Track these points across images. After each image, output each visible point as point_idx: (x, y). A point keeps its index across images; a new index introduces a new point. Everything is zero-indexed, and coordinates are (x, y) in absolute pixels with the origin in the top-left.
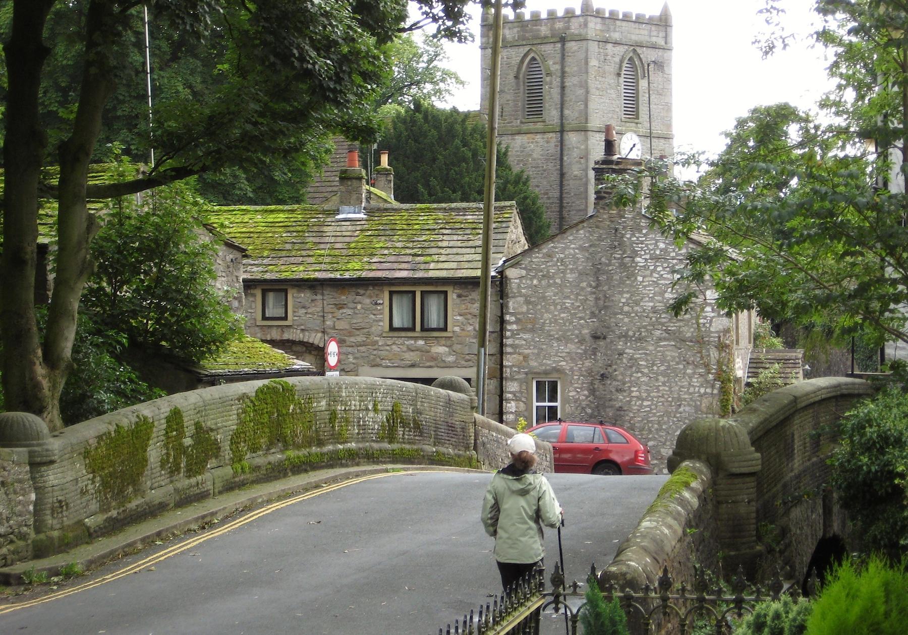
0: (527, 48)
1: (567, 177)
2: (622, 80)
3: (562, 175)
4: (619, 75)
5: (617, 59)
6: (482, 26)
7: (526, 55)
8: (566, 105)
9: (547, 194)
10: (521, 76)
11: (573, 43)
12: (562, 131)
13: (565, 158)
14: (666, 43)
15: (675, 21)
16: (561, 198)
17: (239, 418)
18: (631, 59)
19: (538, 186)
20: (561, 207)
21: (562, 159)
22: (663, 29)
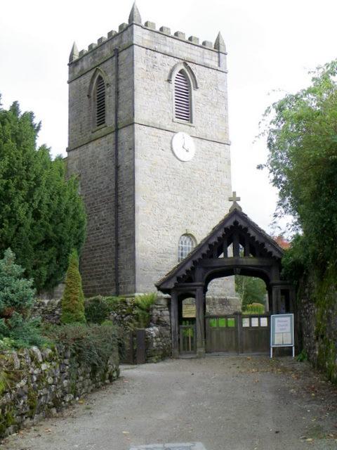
0: (91, 73)
1: (121, 168)
2: (173, 86)
3: (117, 168)
4: (169, 81)
5: (168, 69)
6: (69, 65)
7: (94, 76)
8: (120, 106)
9: (108, 187)
10: (92, 94)
11: (124, 52)
12: (117, 130)
13: (120, 153)
14: (219, 66)
15: (228, 45)
16: (117, 188)
17: (19, 264)
18: (181, 72)
19: (102, 183)
20: (117, 196)
21: (117, 154)
22: (217, 54)
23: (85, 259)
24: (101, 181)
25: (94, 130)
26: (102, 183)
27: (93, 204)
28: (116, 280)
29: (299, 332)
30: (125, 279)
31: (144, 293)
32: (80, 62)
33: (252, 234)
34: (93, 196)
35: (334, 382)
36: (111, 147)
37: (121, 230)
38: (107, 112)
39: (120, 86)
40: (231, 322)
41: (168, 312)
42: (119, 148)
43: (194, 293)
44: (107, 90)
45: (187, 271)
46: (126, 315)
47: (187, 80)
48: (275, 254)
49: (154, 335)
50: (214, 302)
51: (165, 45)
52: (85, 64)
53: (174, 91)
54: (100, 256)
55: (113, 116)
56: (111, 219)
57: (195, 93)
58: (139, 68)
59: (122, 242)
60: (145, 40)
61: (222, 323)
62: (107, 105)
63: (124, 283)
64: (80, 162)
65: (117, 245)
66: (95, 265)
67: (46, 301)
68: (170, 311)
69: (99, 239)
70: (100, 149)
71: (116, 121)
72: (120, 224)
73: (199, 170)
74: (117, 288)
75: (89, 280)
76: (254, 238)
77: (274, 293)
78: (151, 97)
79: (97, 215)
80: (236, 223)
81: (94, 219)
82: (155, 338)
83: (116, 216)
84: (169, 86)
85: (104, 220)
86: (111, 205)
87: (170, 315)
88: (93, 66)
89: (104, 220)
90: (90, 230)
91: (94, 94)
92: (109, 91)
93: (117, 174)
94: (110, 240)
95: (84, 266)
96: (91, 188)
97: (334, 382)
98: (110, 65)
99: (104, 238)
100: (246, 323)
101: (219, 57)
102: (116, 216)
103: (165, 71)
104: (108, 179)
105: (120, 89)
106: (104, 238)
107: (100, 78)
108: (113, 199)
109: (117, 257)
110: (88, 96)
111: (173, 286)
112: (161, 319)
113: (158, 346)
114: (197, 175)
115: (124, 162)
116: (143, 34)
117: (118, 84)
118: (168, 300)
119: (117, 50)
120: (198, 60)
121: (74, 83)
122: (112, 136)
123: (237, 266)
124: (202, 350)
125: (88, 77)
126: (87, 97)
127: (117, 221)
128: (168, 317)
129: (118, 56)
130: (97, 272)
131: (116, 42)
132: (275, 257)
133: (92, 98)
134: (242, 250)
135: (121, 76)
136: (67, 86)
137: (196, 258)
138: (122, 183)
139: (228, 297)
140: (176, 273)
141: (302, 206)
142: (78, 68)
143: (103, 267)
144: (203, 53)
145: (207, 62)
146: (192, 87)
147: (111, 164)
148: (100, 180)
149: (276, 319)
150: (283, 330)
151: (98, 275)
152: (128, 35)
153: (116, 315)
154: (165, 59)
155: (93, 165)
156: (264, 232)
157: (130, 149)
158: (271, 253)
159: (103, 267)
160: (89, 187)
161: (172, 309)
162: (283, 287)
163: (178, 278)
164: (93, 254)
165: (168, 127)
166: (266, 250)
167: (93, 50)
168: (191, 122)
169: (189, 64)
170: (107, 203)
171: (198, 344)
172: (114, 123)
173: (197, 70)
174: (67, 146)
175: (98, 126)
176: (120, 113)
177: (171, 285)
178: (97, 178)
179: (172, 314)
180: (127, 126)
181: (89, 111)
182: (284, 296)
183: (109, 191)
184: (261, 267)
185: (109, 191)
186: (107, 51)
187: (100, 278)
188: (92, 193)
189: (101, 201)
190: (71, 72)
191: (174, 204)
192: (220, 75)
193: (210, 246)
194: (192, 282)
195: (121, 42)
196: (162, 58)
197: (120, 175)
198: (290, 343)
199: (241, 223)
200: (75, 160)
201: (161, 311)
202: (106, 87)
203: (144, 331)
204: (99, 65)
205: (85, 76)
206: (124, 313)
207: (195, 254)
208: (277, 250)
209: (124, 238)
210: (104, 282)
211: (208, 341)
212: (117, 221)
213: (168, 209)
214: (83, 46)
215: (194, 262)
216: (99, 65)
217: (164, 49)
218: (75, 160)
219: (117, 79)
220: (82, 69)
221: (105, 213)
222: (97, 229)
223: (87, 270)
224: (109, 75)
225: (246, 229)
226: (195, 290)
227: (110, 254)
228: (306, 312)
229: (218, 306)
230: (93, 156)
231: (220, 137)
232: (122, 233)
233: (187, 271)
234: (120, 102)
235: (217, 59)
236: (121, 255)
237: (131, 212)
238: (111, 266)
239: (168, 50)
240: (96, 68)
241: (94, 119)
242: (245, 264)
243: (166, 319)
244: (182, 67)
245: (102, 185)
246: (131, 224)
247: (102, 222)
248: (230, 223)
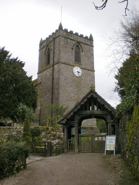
1: (54, 79)
2: (74, 51)
3: (53, 79)
7: (47, 48)
12: (53, 65)
16: (53, 86)
19: (48, 84)
20: (53, 89)
21: (53, 74)
26: (48, 84)
29: (118, 143)
33: (99, 100)
38: (50, 60)
41: (63, 134)
43: (74, 125)
44: (51, 52)
45: (71, 116)
46: (49, 134)
48: (109, 109)
49: (55, 144)
50: (85, 128)
51: (71, 36)
52: (44, 44)
53: (74, 52)
55: (52, 61)
56: (50, 97)
57: (82, 54)
61: (86, 138)
62: (50, 57)
68: (64, 133)
70: (48, 73)
71: (53, 62)
72: (51, 100)
76: (100, 102)
77: (108, 126)
80: (92, 96)
82: (56, 145)
85: (48, 97)
87: (64, 135)
89: (48, 97)
92: (52, 52)
93: (53, 81)
99: (48, 104)
100: (96, 139)
104: (50, 83)
105: (55, 51)
107: (49, 48)
108: (51, 90)
111: (65, 122)
112: (60, 136)
114: (82, 82)
117: (54, 50)
120: (84, 42)
121: (41, 51)
123: (93, 114)
124: (77, 150)
125: (45, 49)
127: (52, 98)
128: (63, 136)
129: (54, 40)
131: (54, 36)
132: (109, 110)
134: (96, 109)
135: (55, 47)
136: (38, 52)
137: (75, 111)
140: (67, 117)
141: (111, 158)
144: (85, 40)
145: (86, 43)
147: (51, 77)
148: (47, 83)
149: (108, 138)
150: (110, 142)
153: (44, 133)
156: (104, 100)
158: (107, 109)
161: (65, 132)
162: (113, 124)
163: (67, 119)
166: (105, 107)
167: (47, 39)
171: (76, 148)
172: (52, 63)
173: (82, 45)
176: (55, 59)
177: (64, 122)
179: (65, 135)
181: (45, 60)
182: (113, 127)
184: (103, 115)
186: (51, 39)
193: (81, 106)
195: (56, 35)
197: (54, 81)
199: (94, 96)
201: (60, 133)
203: (51, 142)
206: (47, 133)
207: (75, 109)
208: (110, 107)
211: (80, 147)
212: (52, 98)
215: (74, 112)
217: (70, 37)
219: (54, 48)
220: (43, 46)
225: (96, 98)
226: (75, 124)
228: (122, 135)
229: (89, 130)
231: (90, 69)
233: (71, 116)
239: (72, 38)
241: (46, 62)
242: (96, 113)
243: (62, 136)
244: (77, 44)
248: (90, 96)
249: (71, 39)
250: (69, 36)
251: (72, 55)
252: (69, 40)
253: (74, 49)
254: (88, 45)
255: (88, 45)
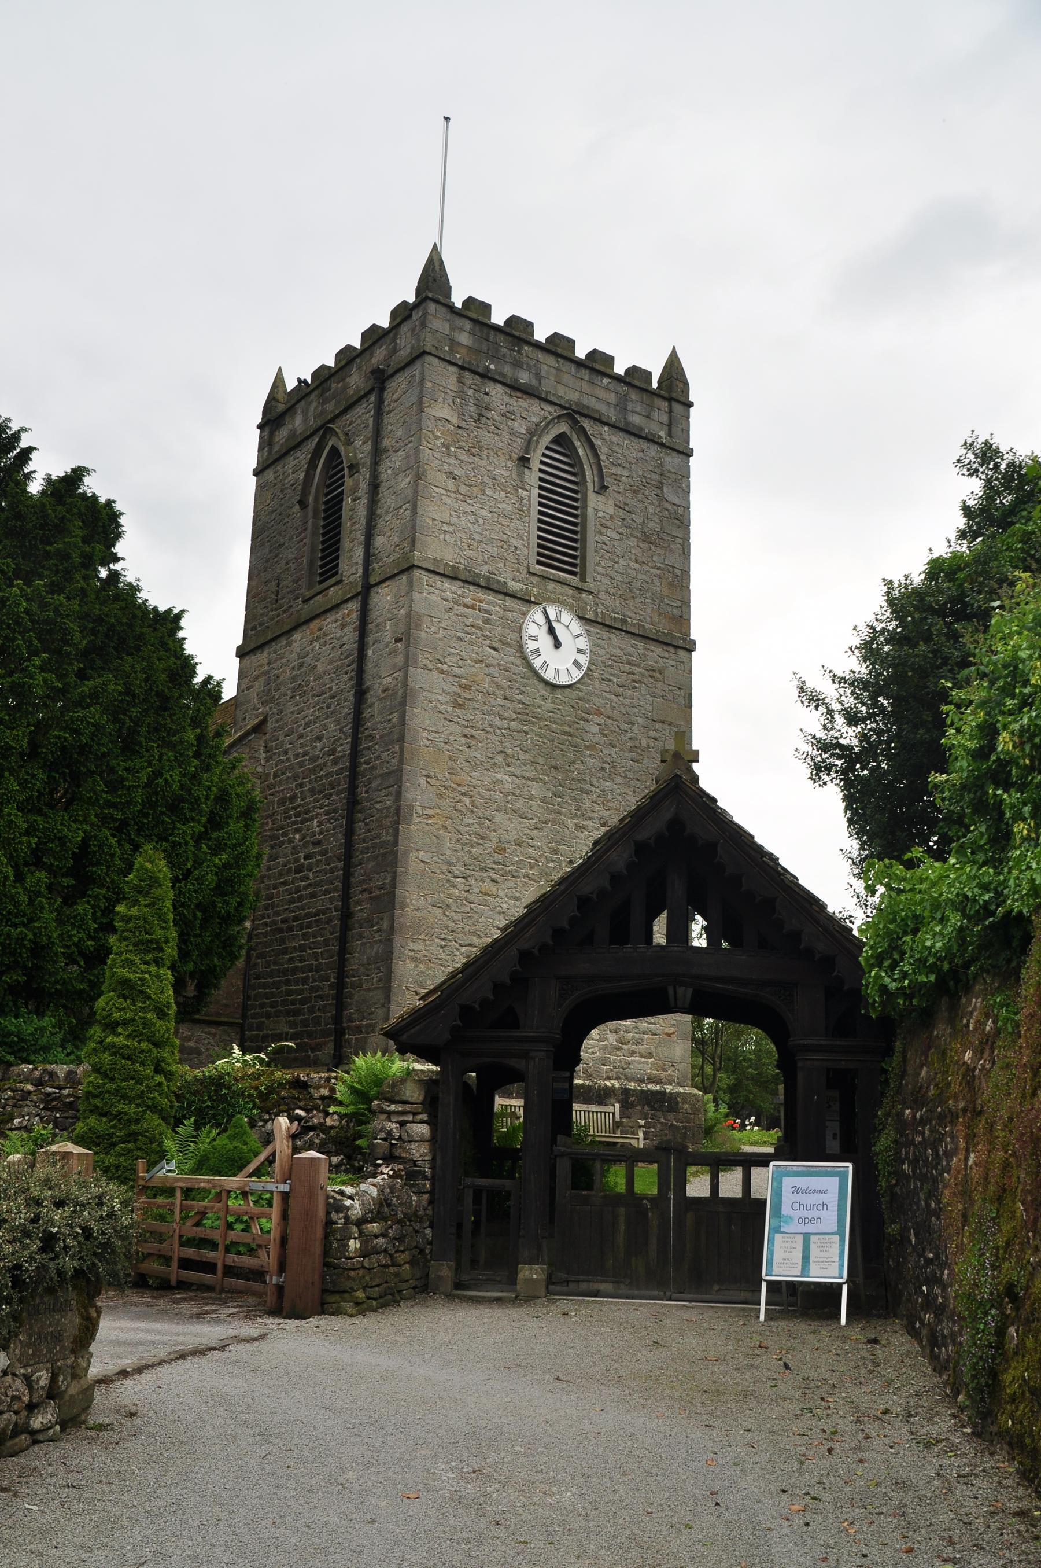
2: (532, 477)
3: (361, 693)
4: (524, 461)
14: (670, 434)
18: (560, 440)
19: (319, 738)
23: (261, 956)
24: (317, 732)
25: (308, 594)
27: (293, 799)
28: (338, 1019)
30: (363, 1018)
31: (618, 1078)
32: (287, 419)
34: (295, 778)
35: (1033, 1453)
36: (350, 636)
37: (358, 873)
38: (346, 544)
39: (381, 468)
40: (647, 1180)
42: (370, 639)
45: (497, 987)
47: (576, 461)
53: (536, 491)
54: (302, 948)
55: (359, 553)
56: (335, 843)
57: (598, 506)
58: (438, 419)
59: (361, 910)
60: (459, 344)
62: (346, 524)
63: (358, 1030)
64: (267, 683)
65: (346, 915)
66: (285, 972)
67: (61, 1070)
69: (300, 898)
73: (599, 713)
74: (339, 1046)
75: (268, 1016)
78: (462, 493)
79: (298, 830)
81: (290, 841)
82: (360, 1222)
83: (350, 832)
84: (521, 475)
86: (339, 800)
88: (319, 423)
89: (318, 843)
90: (281, 874)
91: (316, 499)
94: (328, 902)
95: (258, 977)
96: (291, 754)
97: (1033, 1453)
98: (363, 414)
99: (313, 895)
100: (698, 1186)
101: (670, 411)
102: (350, 832)
103: (512, 432)
104: (335, 730)
105: (384, 477)
106: (313, 895)
107: (335, 452)
109: (343, 951)
110: (300, 502)
113: (364, 1253)
114: (595, 729)
115: (382, 674)
116: (453, 328)
118: (430, 1084)
119: (383, 371)
122: (354, 606)
125: (303, 456)
126: (297, 507)
127: (349, 845)
129: (382, 389)
130: (289, 993)
131: (380, 354)
133: (310, 508)
138: (371, 737)
139: (669, 1089)
142: (282, 435)
143: (304, 981)
145: (636, 420)
146: (590, 486)
147: (345, 683)
148: (315, 729)
151: (293, 1003)
152: (413, 330)
154: (513, 401)
155: (300, 690)
157: (398, 640)
159: (304, 981)
160: (286, 752)
164: (283, 941)
165: (514, 586)
168: (583, 580)
169: (586, 424)
170: (328, 797)
173: (604, 438)
174: (240, 641)
175: (320, 582)
176: (380, 541)
178: (307, 725)
180: (392, 577)
181: (299, 550)
183: (335, 762)
185: (335, 762)
187: (297, 1013)
188: (290, 768)
189: (312, 791)
190: (265, 444)
191: (519, 804)
192: (671, 461)
194: (516, 1025)
196: (506, 398)
197: (366, 714)
198: (835, 1181)
200: (257, 678)
201: (402, 1124)
202: (346, 471)
204: (329, 422)
205: (299, 454)
209: (366, 895)
210: (305, 1023)
212: (349, 845)
213: (498, 817)
214: (299, 370)
216: (332, 420)
218: (257, 678)
221: (320, 824)
222: (298, 870)
223: (265, 986)
224: (358, 443)
227: (326, 943)
230: (302, 665)
232: (361, 882)
233: (497, 987)
234: (379, 511)
235: (665, 418)
236: (356, 944)
237: (387, 822)
238: (327, 980)
239: (524, 378)
240: (325, 430)
241: (311, 563)
244: (563, 427)
245: (319, 745)
246: (389, 858)
247: (311, 849)
249: (514, 387)
250: (495, 357)
251: (521, 512)
252: (497, 392)
253: (535, 465)
254: (651, 439)
255: (651, 439)
